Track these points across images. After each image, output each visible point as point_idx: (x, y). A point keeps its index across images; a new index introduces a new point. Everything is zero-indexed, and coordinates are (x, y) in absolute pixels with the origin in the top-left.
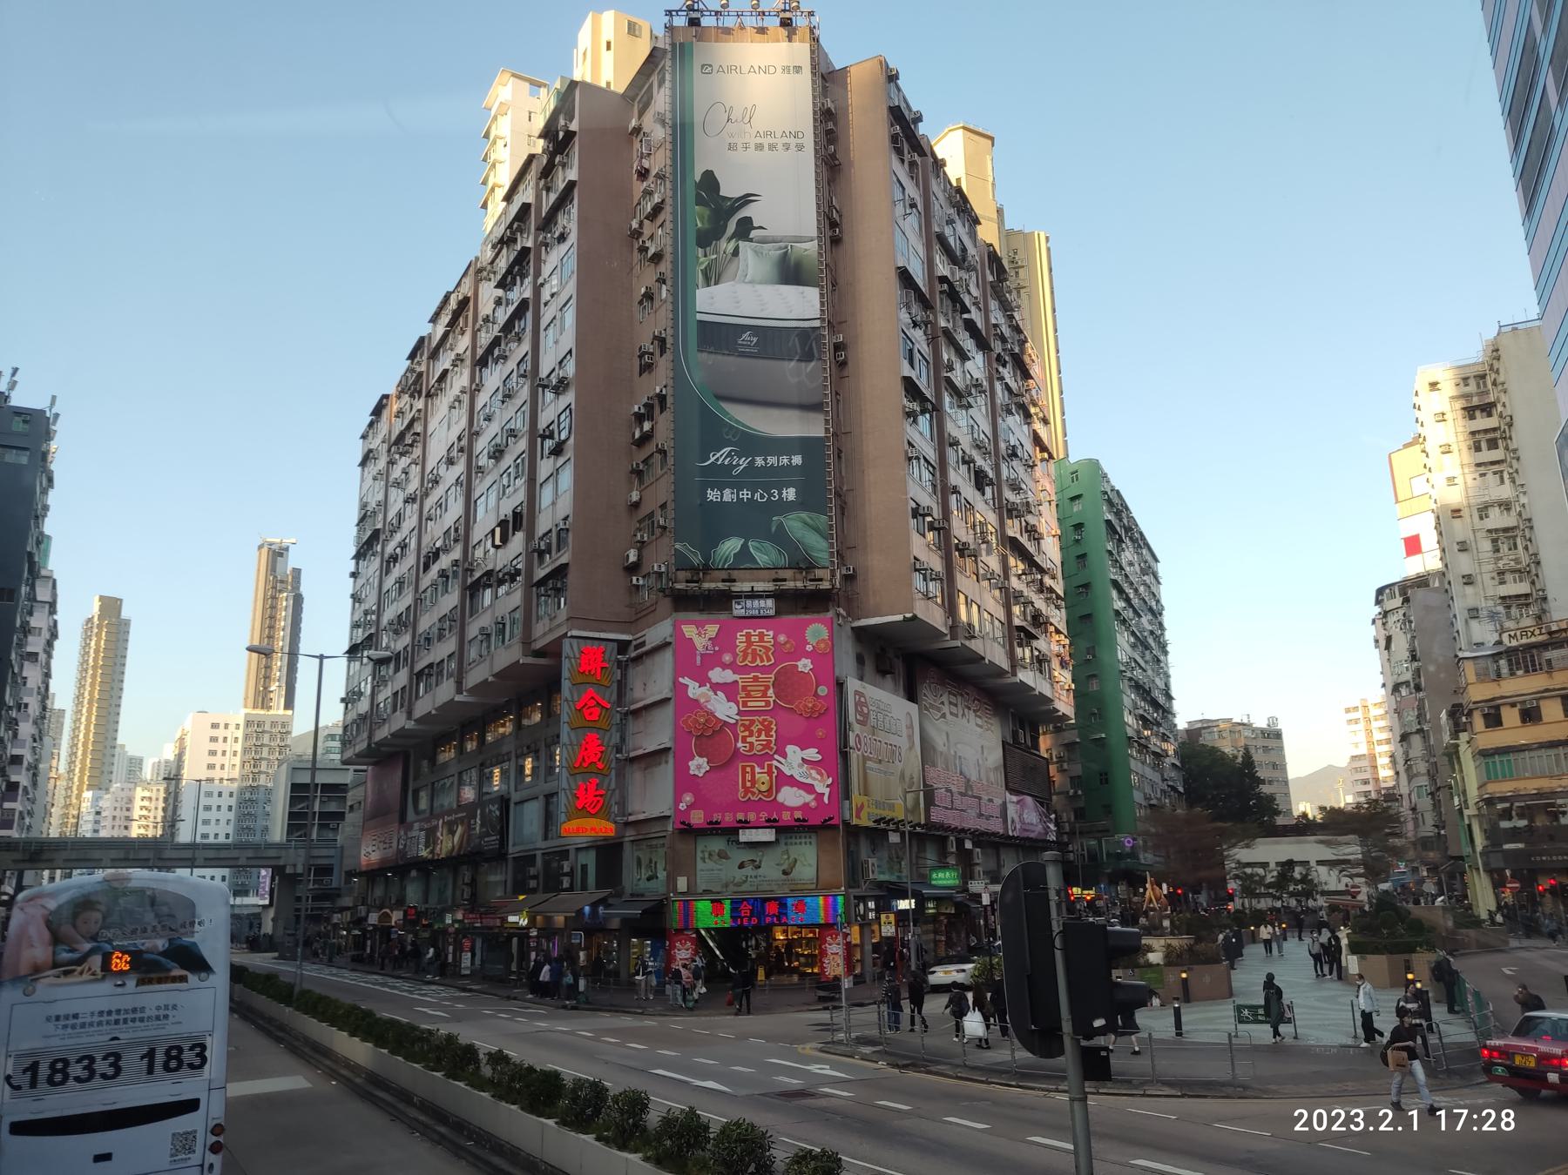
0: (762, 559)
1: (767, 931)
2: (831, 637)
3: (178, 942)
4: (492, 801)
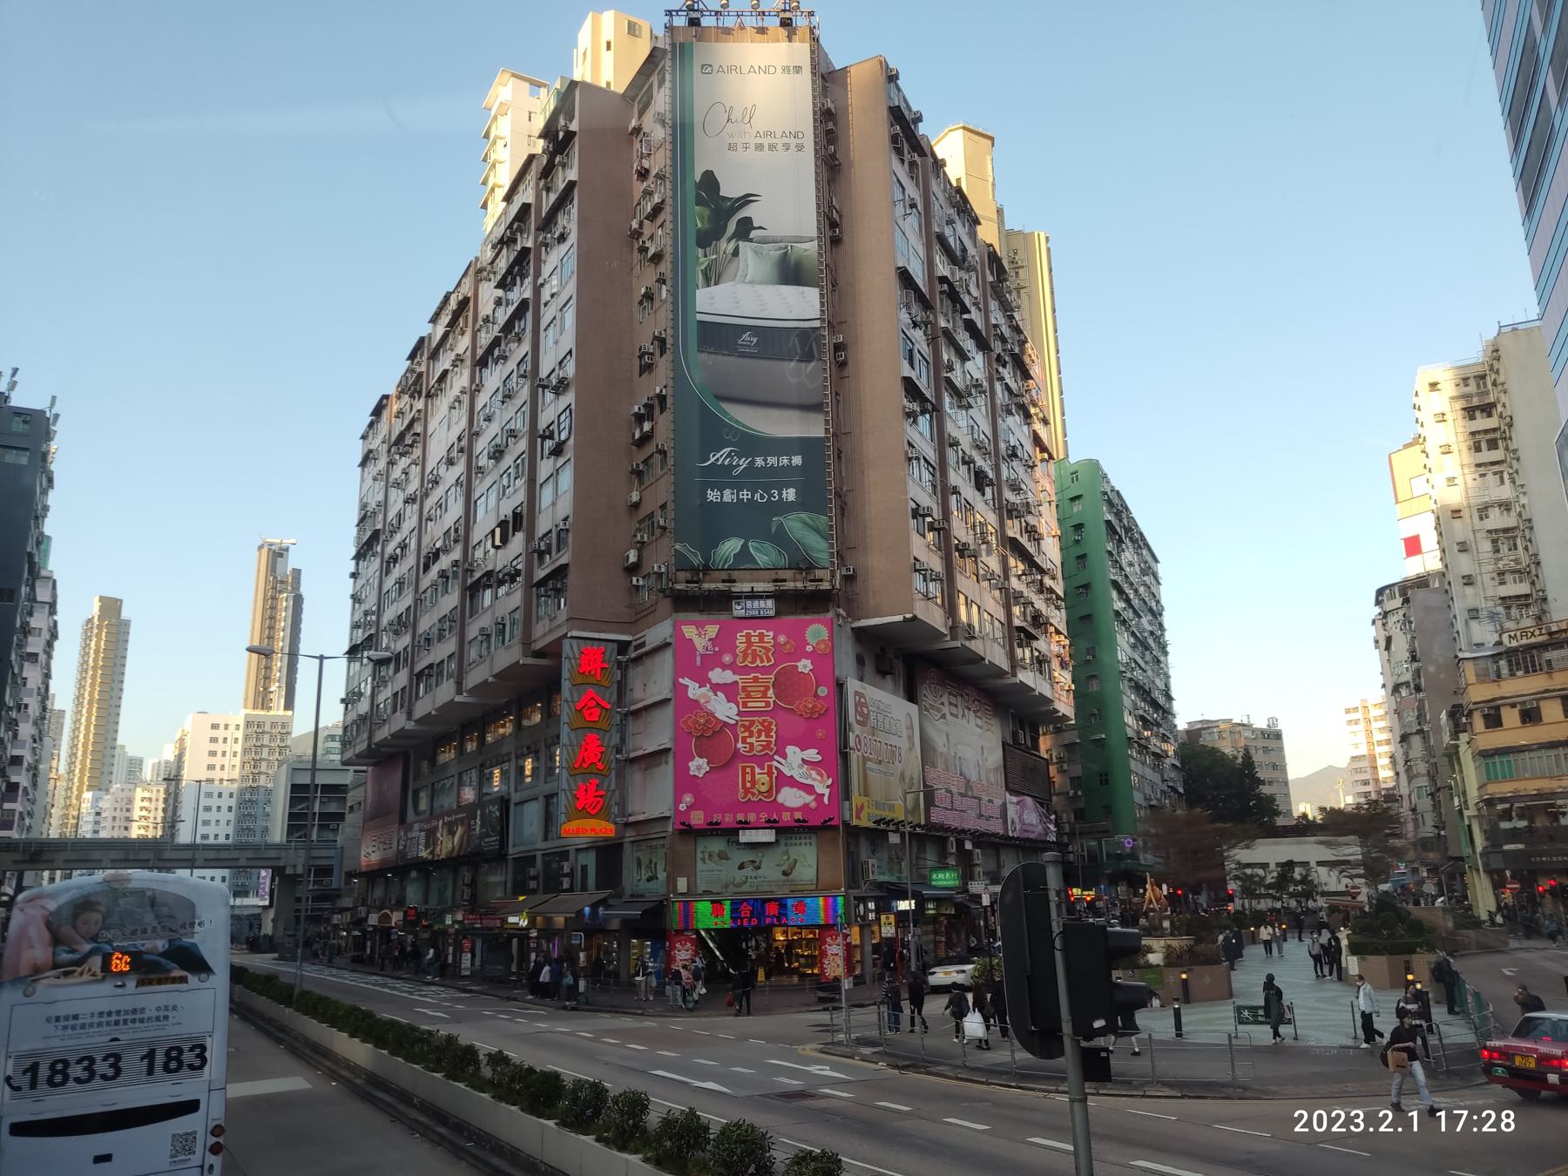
0: (762, 559)
1: (767, 931)
2: (831, 638)
3: (178, 943)
4: (492, 802)
